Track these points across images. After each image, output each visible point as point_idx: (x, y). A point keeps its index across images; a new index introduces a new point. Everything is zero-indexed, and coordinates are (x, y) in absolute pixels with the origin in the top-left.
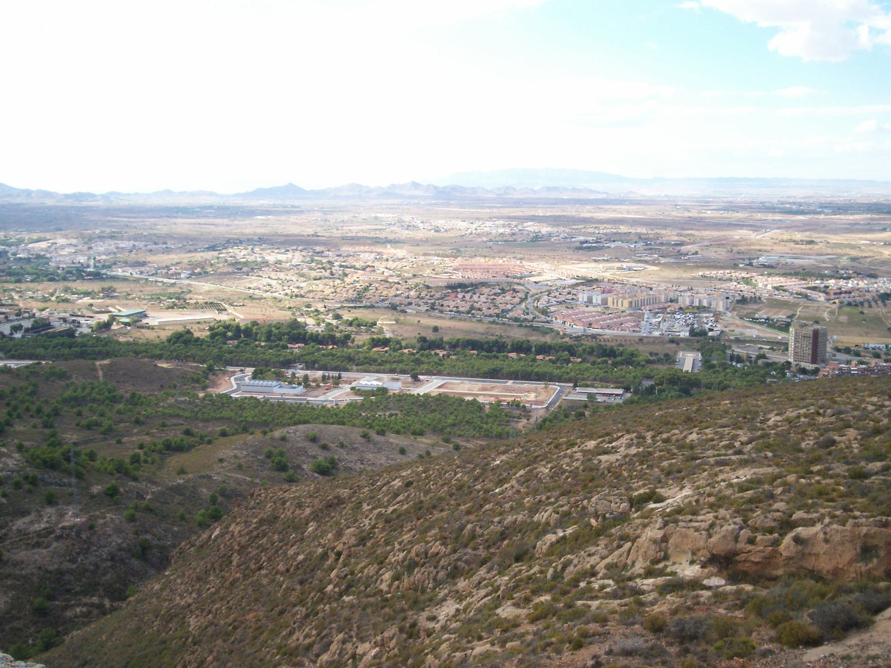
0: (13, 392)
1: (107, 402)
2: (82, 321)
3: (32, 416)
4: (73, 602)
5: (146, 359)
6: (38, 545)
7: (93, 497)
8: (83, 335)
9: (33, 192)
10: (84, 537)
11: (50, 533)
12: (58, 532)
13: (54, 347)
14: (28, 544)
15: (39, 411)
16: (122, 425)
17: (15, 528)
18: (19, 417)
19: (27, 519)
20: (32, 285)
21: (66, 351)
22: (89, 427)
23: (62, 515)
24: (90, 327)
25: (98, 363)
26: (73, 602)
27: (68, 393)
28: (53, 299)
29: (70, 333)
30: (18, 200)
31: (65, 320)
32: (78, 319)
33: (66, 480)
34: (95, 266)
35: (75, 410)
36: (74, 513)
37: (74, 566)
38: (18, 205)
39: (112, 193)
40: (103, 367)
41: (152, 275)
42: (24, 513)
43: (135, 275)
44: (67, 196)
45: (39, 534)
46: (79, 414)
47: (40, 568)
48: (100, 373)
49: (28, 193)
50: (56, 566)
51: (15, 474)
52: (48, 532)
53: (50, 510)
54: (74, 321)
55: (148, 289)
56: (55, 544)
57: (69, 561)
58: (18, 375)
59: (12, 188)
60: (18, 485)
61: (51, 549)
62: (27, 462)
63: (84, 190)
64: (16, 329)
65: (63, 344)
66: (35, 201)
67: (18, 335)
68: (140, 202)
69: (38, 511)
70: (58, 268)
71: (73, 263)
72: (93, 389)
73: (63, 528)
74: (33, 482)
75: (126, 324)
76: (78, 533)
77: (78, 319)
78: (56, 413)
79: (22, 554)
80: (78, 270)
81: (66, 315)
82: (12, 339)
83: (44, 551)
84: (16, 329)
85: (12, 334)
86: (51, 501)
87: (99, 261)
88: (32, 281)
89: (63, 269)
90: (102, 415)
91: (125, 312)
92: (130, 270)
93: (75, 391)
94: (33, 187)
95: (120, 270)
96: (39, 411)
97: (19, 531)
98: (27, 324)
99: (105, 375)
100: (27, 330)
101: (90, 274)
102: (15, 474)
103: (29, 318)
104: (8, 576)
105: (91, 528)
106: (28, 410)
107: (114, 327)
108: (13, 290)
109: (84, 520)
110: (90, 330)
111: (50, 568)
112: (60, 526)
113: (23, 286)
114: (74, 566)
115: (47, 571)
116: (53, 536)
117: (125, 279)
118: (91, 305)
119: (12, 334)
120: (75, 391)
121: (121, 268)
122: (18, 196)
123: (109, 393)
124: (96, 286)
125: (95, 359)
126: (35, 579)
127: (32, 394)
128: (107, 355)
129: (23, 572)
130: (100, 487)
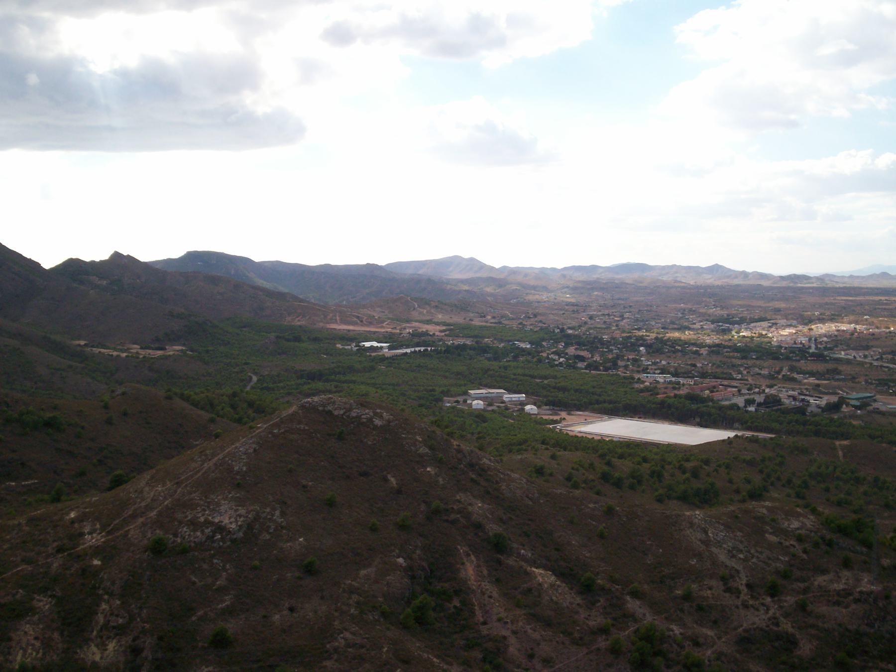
0: (763, 460)
1: (852, 482)
2: (437, 388)
3: (783, 486)
4: (870, 664)
5: (884, 445)
6: (837, 603)
7: (884, 568)
8: (814, 415)
9: (750, 273)
10: (881, 604)
11: (850, 594)
12: (857, 595)
13: (789, 423)
14: (829, 601)
15: (789, 482)
16: (871, 507)
17: (816, 583)
18: (772, 484)
19: (826, 577)
20: (758, 362)
21: (801, 428)
22: (839, 504)
23: (858, 580)
24: (818, 406)
25: (837, 443)
26: (870, 664)
27: (813, 469)
28: (780, 377)
29: (801, 411)
30: (736, 282)
31: (795, 399)
32: (808, 398)
33: (858, 548)
34: (817, 348)
35: (822, 486)
36: (869, 581)
37: (872, 631)
38: (738, 286)
39: (827, 275)
40: (843, 448)
41: (877, 360)
42: (824, 572)
43: (858, 359)
44: (782, 278)
45: (838, 593)
46: (827, 490)
47: (840, 625)
48: (840, 453)
49: (745, 274)
50: (855, 627)
51: (813, 534)
52: (847, 593)
53: (846, 573)
54: (803, 400)
55: (674, 363)
56: (854, 606)
57: (867, 625)
58: (765, 445)
59: (729, 270)
60: (816, 545)
61: (850, 609)
62: (822, 524)
63: (799, 272)
64: (749, 402)
65: (797, 421)
66: (708, 280)
67: (752, 409)
68: (856, 284)
69: (837, 572)
70: (781, 347)
71: (795, 343)
72: (835, 468)
73: (861, 592)
74: (830, 544)
75: (857, 407)
76: (875, 601)
77: (808, 398)
78: (805, 485)
79: (823, 609)
80: (800, 349)
81: (795, 393)
82: (747, 411)
83: (844, 610)
84: (749, 402)
85: (745, 407)
86: (847, 564)
87: (821, 343)
88: (757, 359)
89: (786, 348)
90: (849, 494)
91: (854, 395)
92: (854, 353)
93: (819, 468)
94: (749, 270)
95: (843, 353)
96: (789, 482)
97: (820, 587)
98: (760, 399)
99: (844, 456)
100: (759, 405)
101: (813, 355)
102: (813, 534)
103: (759, 393)
104: (813, 626)
105: (887, 597)
106: (779, 479)
107: (844, 408)
108: (742, 365)
109: (879, 589)
110: (820, 410)
111: (849, 627)
112: (858, 590)
113: (750, 362)
114: (872, 631)
115: (847, 629)
116: (851, 598)
117: (848, 362)
118: (818, 385)
119: (745, 407)
120: (819, 468)
121: (844, 350)
122: (736, 277)
123: (852, 473)
124: (820, 367)
125: (837, 439)
126: (836, 634)
127: (781, 464)
128: (844, 436)
129: (826, 626)
130: (888, 561)
